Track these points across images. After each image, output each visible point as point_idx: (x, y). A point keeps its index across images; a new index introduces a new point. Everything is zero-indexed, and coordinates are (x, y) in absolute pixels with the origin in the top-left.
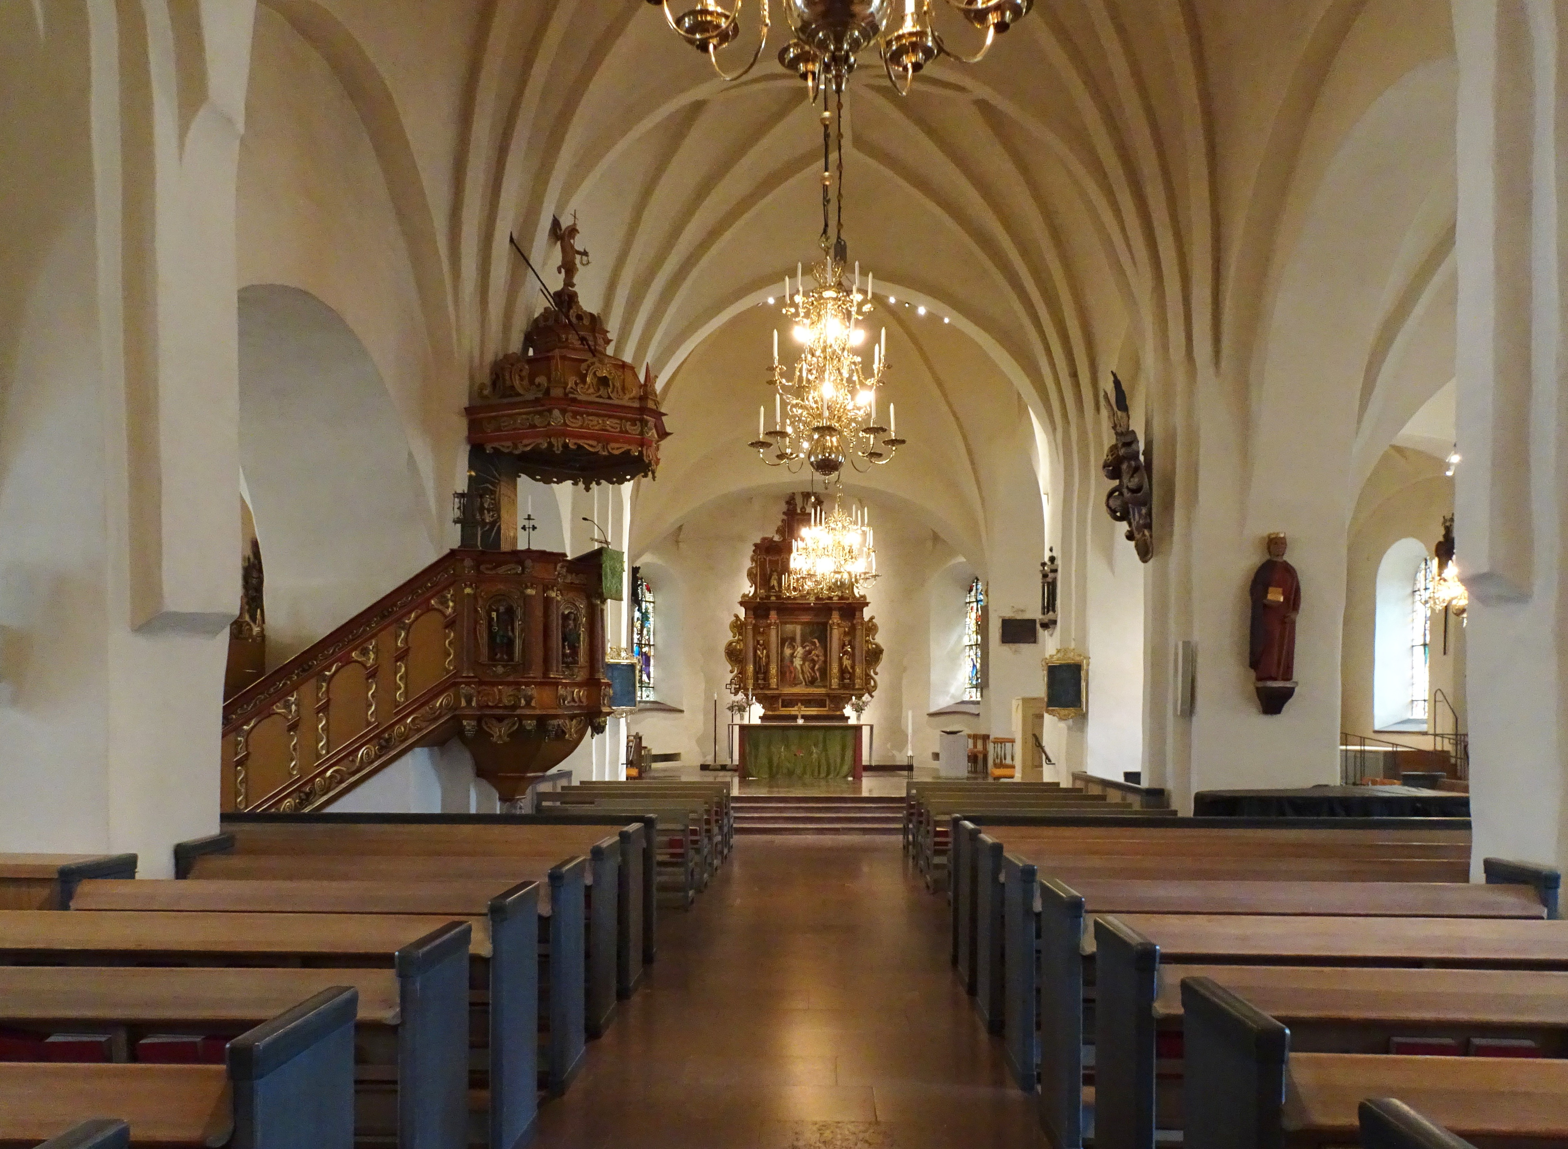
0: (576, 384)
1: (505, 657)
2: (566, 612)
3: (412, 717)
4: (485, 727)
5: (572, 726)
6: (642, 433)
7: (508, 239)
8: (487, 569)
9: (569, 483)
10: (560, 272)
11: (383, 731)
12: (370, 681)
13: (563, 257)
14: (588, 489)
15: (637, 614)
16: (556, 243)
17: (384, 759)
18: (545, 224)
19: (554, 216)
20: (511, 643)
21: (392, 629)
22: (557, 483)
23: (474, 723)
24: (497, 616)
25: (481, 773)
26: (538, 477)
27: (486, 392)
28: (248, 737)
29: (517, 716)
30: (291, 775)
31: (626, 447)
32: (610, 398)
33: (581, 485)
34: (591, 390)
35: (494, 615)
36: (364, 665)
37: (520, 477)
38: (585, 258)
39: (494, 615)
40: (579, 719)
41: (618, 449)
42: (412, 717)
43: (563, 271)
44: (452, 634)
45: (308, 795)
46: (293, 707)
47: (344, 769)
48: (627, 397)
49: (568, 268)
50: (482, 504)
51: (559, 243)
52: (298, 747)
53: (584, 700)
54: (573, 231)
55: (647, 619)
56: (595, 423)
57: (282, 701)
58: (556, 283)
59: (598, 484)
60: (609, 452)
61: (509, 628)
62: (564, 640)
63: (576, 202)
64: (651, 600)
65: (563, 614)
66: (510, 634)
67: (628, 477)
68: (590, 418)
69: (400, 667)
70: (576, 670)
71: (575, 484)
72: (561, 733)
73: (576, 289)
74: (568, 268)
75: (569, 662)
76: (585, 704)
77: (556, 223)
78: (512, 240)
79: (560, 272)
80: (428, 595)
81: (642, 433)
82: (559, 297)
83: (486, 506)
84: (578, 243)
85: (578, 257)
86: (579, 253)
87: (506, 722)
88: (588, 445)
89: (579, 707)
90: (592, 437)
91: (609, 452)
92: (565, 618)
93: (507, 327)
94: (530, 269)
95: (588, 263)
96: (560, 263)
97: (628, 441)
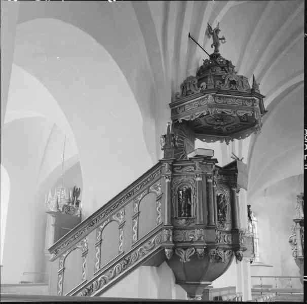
0: (220, 84)
1: (187, 215)
2: (219, 195)
3: (140, 248)
4: (177, 253)
5: (225, 255)
6: (253, 105)
7: (188, 36)
8: (177, 169)
9: (219, 141)
10: (212, 47)
11: (126, 255)
12: (121, 230)
13: (214, 41)
14: (228, 144)
15: (250, 225)
16: (209, 37)
17: (126, 271)
18: (204, 28)
19: (208, 24)
20: (189, 207)
21: (131, 203)
22: (213, 142)
23: (171, 250)
24: (182, 193)
25: (178, 281)
26: (204, 140)
27: (178, 96)
28: (65, 259)
29: (193, 246)
30: (82, 280)
31: (246, 112)
32: (236, 89)
33: (224, 142)
34: (227, 87)
35: (181, 192)
36: (118, 221)
37: (195, 140)
38: (223, 41)
39: (181, 192)
40: (228, 251)
41: (242, 113)
42: (140, 248)
43: (213, 46)
44: (160, 204)
45: (89, 290)
46: (85, 245)
47: (107, 276)
48: (245, 89)
49: (216, 45)
50: (174, 139)
51: (212, 36)
52: (86, 265)
53: (230, 240)
54: (217, 31)
55: (255, 228)
56: (230, 101)
57: (81, 242)
58: (211, 51)
59: (233, 141)
60: (237, 115)
61: (189, 199)
62: (218, 209)
63: (219, 19)
64: (256, 220)
65: (217, 196)
66: (189, 202)
67: (247, 135)
68: (227, 99)
69: (135, 222)
70: (225, 225)
71: (222, 142)
72: (219, 259)
73: (219, 52)
74: (216, 45)
75: (222, 220)
76: (231, 243)
77: (209, 28)
78: (189, 36)
79: (212, 47)
80: (149, 185)
81: (253, 105)
82: (212, 56)
83: (176, 139)
84: (220, 35)
85: (220, 41)
86: (220, 39)
87: (188, 250)
88: (227, 111)
89: (228, 245)
90: (229, 107)
91: (237, 115)
92: (219, 197)
93: (188, 66)
94: (198, 45)
95: (225, 42)
96: (212, 43)
97: (247, 109)
